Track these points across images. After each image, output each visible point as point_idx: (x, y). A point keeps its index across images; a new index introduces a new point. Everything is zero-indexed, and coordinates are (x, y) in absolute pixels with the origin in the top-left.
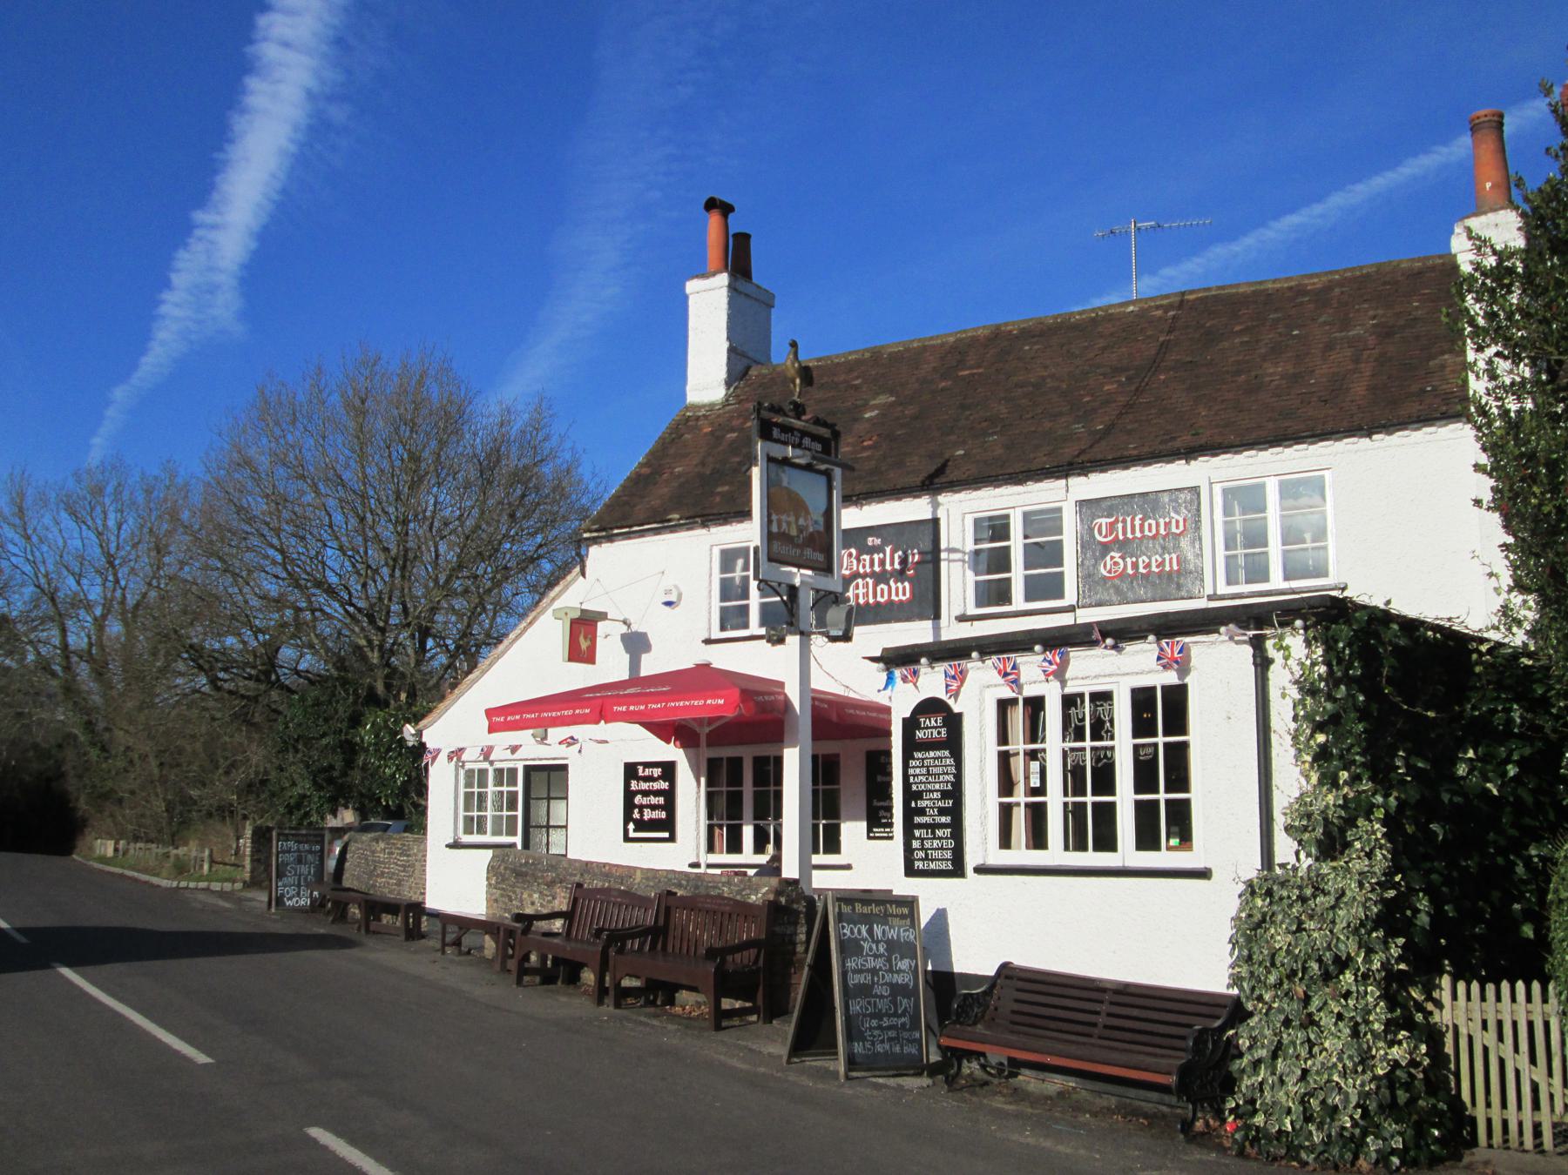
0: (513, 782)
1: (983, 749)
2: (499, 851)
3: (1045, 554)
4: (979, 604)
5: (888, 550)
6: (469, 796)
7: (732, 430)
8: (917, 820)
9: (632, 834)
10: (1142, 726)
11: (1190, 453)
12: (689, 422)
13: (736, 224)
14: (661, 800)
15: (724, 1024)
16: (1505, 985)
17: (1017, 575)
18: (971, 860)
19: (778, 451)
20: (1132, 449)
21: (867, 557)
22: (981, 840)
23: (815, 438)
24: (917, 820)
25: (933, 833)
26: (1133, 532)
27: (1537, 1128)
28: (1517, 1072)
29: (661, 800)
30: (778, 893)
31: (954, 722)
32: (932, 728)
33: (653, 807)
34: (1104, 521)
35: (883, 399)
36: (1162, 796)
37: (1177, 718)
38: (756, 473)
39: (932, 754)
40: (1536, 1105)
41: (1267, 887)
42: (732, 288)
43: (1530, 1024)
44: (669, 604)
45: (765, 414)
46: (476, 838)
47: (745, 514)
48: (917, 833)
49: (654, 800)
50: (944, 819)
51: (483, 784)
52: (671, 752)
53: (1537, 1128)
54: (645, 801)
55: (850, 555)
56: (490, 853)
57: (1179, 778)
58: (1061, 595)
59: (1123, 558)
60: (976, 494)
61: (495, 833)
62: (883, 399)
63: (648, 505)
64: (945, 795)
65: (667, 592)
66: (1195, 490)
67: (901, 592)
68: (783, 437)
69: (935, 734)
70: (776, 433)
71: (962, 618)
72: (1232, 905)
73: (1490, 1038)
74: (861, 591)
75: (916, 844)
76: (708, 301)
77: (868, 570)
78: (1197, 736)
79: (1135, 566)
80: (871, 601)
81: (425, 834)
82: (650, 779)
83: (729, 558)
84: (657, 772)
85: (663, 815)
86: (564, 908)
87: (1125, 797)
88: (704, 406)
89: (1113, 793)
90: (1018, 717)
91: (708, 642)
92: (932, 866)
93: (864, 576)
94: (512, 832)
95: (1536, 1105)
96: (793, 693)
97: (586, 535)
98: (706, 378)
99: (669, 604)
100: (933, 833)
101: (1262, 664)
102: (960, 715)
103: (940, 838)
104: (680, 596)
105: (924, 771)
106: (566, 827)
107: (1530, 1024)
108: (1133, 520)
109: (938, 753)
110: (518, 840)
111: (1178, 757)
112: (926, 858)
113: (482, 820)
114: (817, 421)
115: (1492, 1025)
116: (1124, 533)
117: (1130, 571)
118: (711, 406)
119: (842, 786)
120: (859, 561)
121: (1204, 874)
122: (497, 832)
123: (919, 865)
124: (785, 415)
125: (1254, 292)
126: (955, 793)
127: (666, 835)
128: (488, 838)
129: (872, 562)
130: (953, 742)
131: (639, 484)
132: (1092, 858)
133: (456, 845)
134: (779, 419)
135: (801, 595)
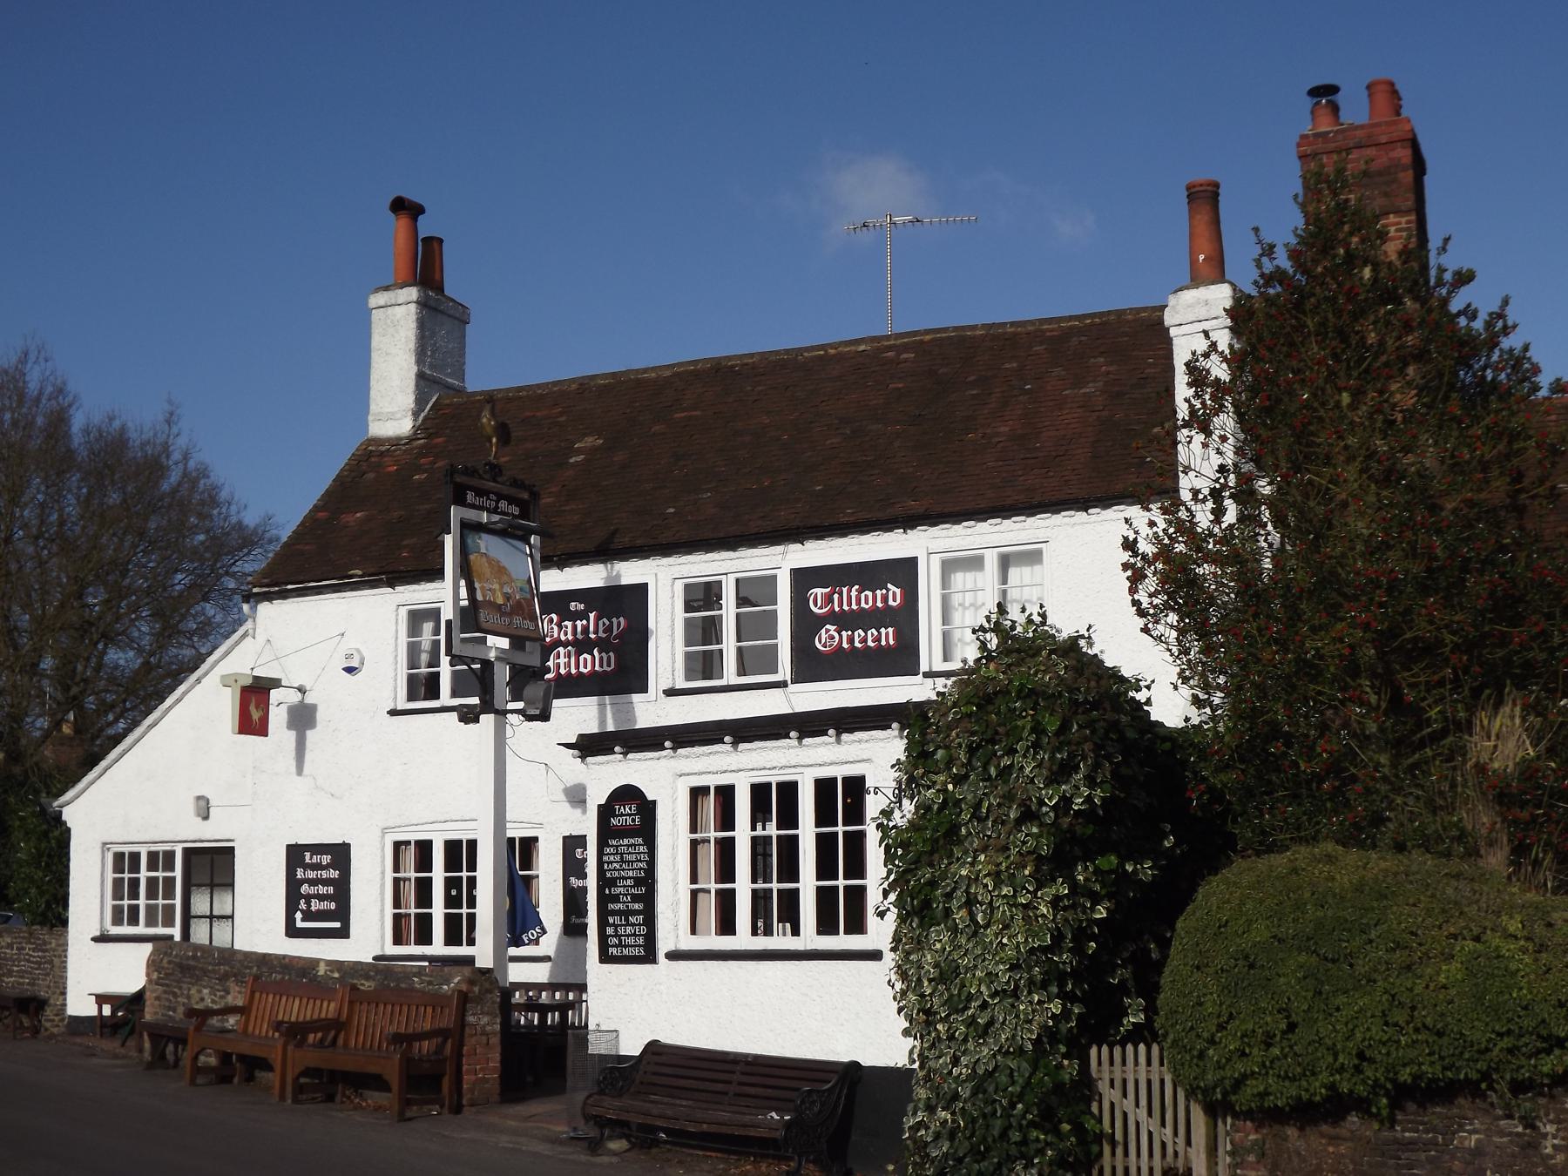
0: (170, 866)
2: (162, 943)
3: (756, 626)
4: (688, 679)
5: (592, 616)
6: (118, 884)
7: (418, 470)
8: (611, 906)
9: (300, 924)
10: (824, 814)
11: (908, 522)
12: (373, 455)
13: (426, 227)
14: (331, 890)
15: (408, 1114)
17: (729, 645)
18: (664, 945)
19: (471, 515)
21: (569, 624)
22: (672, 928)
23: (512, 501)
24: (611, 906)
25: (627, 920)
26: (849, 604)
28: (1138, 1124)
30: (471, 982)
31: (648, 809)
32: (627, 815)
33: (321, 898)
34: (819, 591)
35: (590, 441)
36: (841, 882)
38: (449, 541)
39: (626, 841)
42: (422, 304)
44: (350, 670)
45: (459, 479)
46: (126, 930)
47: (436, 574)
48: (611, 920)
49: (322, 890)
50: (636, 906)
51: (135, 867)
54: (312, 890)
55: (551, 621)
56: (148, 948)
60: (685, 559)
62: (590, 441)
63: (329, 554)
64: (638, 882)
65: (349, 657)
66: (913, 562)
68: (478, 501)
69: (629, 821)
70: (470, 497)
71: (671, 692)
74: (562, 660)
75: (610, 931)
76: (395, 325)
77: (570, 637)
79: (851, 640)
80: (573, 671)
82: (317, 867)
83: (417, 618)
84: (326, 859)
85: (333, 906)
86: (240, 1003)
87: (808, 883)
89: (797, 881)
90: (710, 805)
91: (394, 713)
92: (626, 952)
93: (565, 644)
94: (169, 922)
97: (255, 590)
98: (392, 409)
99: (350, 670)
100: (627, 920)
102: (654, 802)
103: (633, 925)
105: (618, 858)
106: (232, 917)
107: (1149, 1082)
108: (849, 591)
109: (632, 841)
110: (176, 932)
112: (620, 945)
113: (134, 910)
114: (515, 483)
115: (1118, 1084)
116: (841, 604)
117: (845, 645)
118: (395, 442)
120: (560, 627)
122: (151, 922)
123: (613, 951)
124: (481, 478)
126: (648, 881)
127: (337, 925)
128: (141, 929)
129: (575, 627)
130: (646, 829)
131: (312, 527)
133: (103, 938)
134: (475, 482)
135: (497, 667)
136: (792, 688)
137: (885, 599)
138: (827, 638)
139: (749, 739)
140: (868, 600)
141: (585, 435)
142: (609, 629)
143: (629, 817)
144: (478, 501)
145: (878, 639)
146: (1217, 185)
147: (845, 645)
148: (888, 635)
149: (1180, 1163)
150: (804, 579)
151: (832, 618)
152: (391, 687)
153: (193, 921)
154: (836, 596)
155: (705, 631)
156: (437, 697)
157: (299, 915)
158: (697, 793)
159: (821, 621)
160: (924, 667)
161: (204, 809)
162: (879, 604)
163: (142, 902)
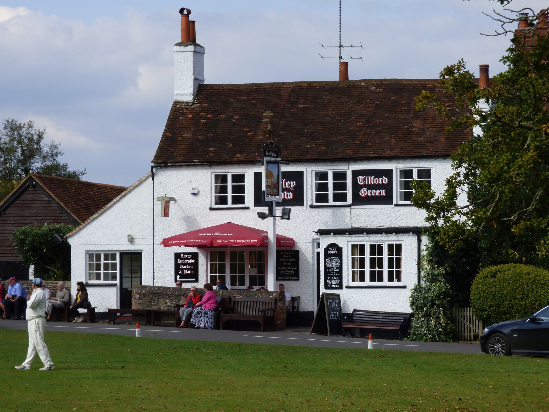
1: (348, 257)
3: (340, 186)
8: (328, 274)
9: (178, 279)
10: (372, 252)
11: (390, 158)
13: (191, 18)
14: (192, 267)
16: (466, 309)
18: (345, 284)
20: (371, 154)
21: (287, 187)
22: (347, 279)
26: (371, 182)
27: (470, 336)
29: (192, 267)
31: (340, 250)
33: (188, 269)
34: (361, 177)
36: (377, 269)
37: (399, 252)
40: (470, 332)
41: (418, 289)
43: (470, 316)
49: (188, 267)
52: (194, 250)
53: (470, 336)
54: (184, 267)
57: (399, 265)
58: (345, 200)
59: (367, 190)
61: (105, 280)
64: (337, 268)
66: (391, 171)
67: (289, 196)
68: (270, 154)
70: (267, 153)
72: (410, 293)
73: (462, 319)
75: (328, 281)
78: (404, 256)
79: (371, 193)
81: (70, 280)
82: (187, 259)
84: (189, 256)
85: (193, 272)
88: (183, 103)
91: (211, 209)
92: (333, 286)
95: (470, 332)
96: (271, 237)
101: (419, 241)
104: (199, 191)
107: (470, 316)
111: (399, 260)
116: (368, 182)
118: (187, 103)
119: (226, 262)
121: (405, 287)
122: (106, 278)
125: (408, 84)
126: (340, 268)
127: (194, 279)
132: (358, 283)
136: (353, 207)
137: (382, 181)
138: (363, 192)
139: (371, 234)
140: (377, 181)
141: (267, 110)
142: (290, 185)
143: (334, 252)
144: (270, 154)
145: (380, 193)
146: (488, 66)
147: (369, 195)
148: (383, 192)
149: (476, 334)
150: (356, 174)
151: (365, 186)
152: (210, 200)
153: (124, 279)
154: (366, 179)
155: (322, 187)
156: (227, 204)
157: (178, 276)
158: (354, 247)
159: (362, 187)
160: (394, 202)
161: (131, 240)
162: (380, 183)
163: (102, 272)
